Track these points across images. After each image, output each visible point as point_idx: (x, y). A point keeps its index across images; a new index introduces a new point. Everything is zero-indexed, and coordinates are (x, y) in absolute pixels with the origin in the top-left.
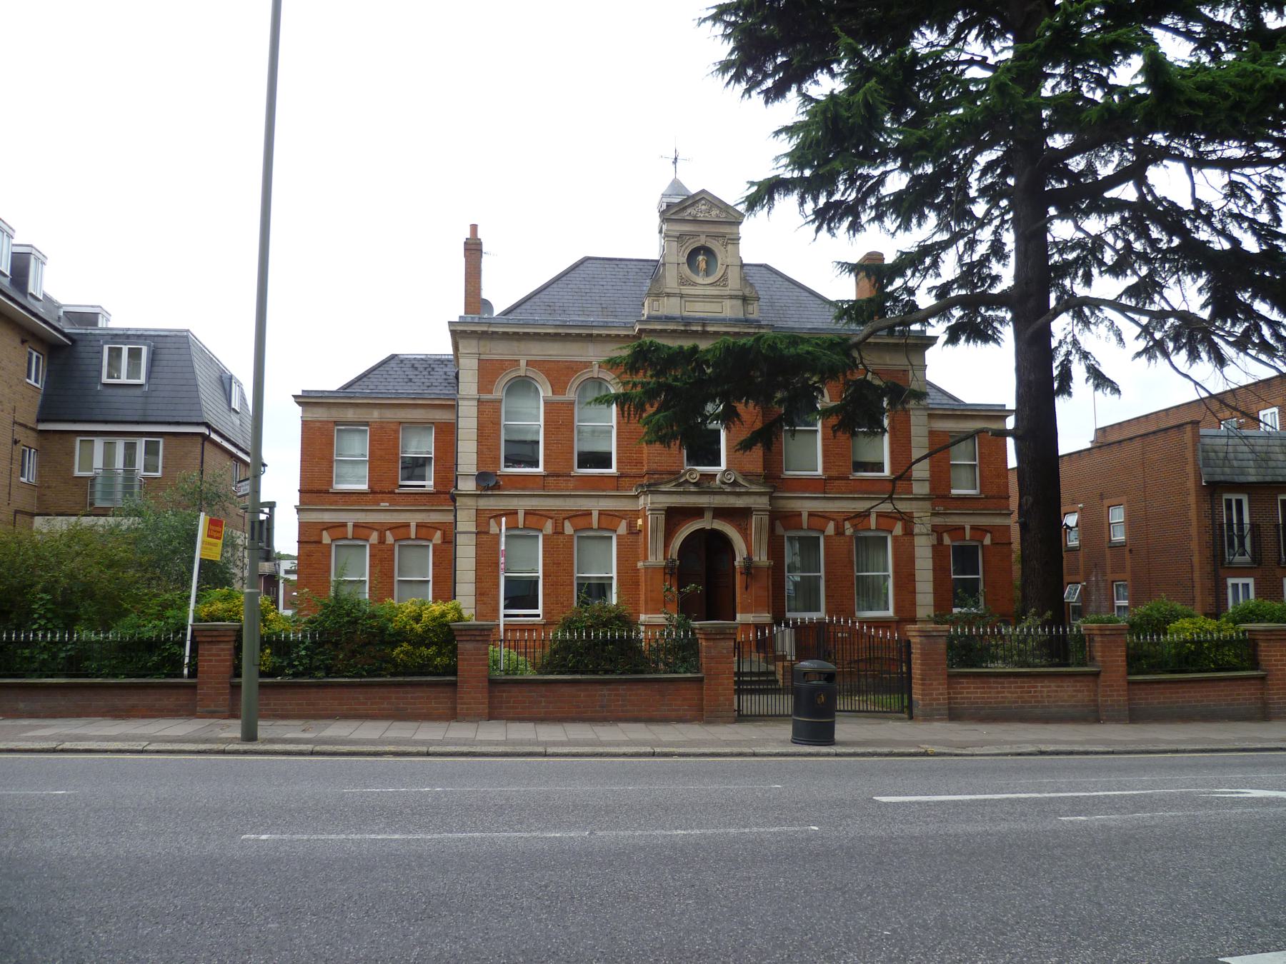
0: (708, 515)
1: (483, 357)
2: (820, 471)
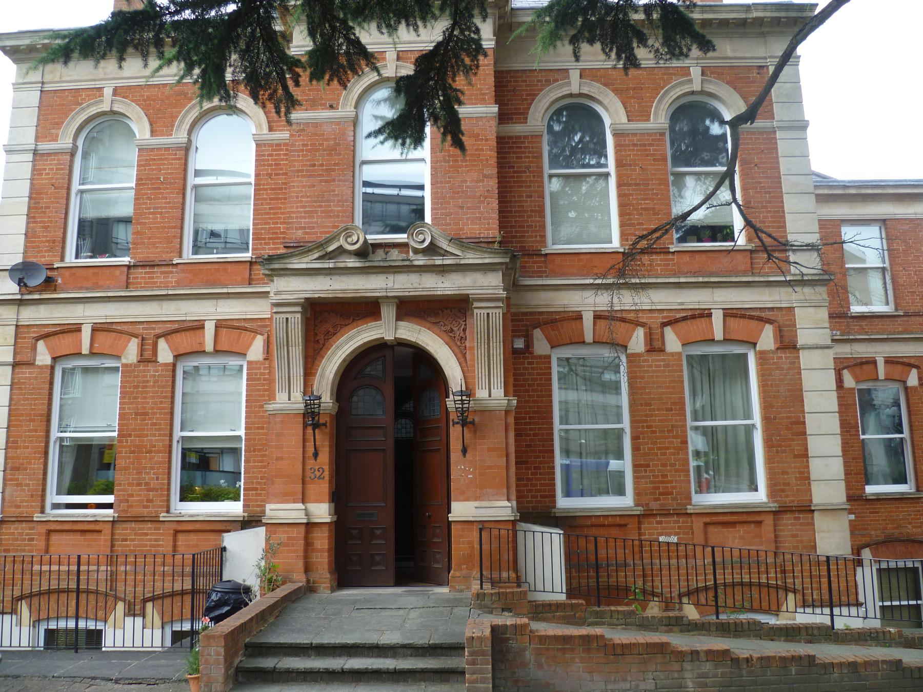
0: (388, 312)
1: (48, 87)
2: (616, 244)
